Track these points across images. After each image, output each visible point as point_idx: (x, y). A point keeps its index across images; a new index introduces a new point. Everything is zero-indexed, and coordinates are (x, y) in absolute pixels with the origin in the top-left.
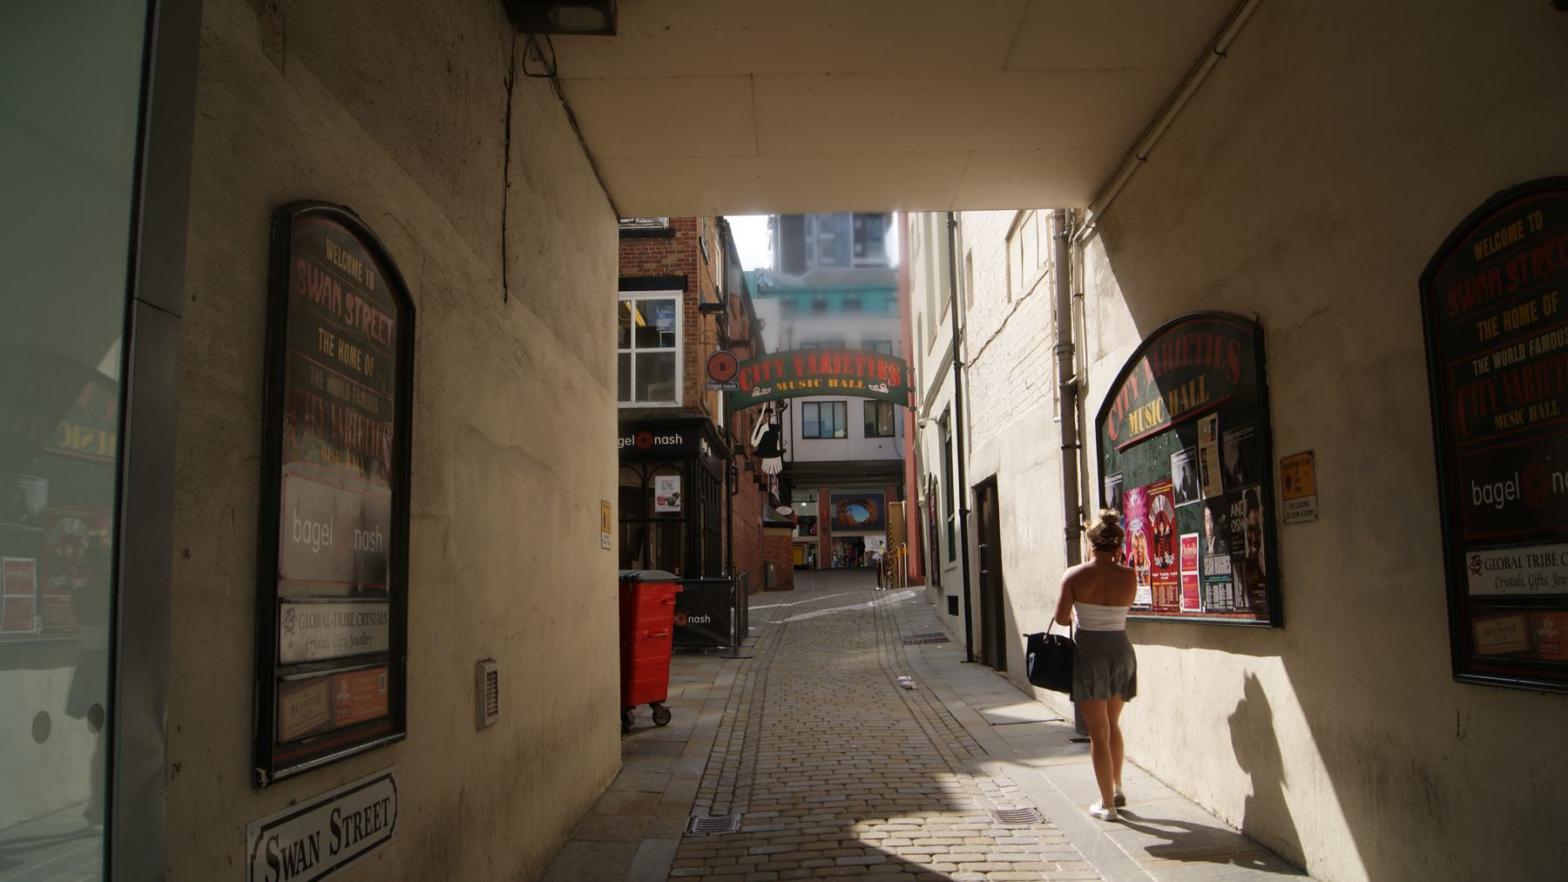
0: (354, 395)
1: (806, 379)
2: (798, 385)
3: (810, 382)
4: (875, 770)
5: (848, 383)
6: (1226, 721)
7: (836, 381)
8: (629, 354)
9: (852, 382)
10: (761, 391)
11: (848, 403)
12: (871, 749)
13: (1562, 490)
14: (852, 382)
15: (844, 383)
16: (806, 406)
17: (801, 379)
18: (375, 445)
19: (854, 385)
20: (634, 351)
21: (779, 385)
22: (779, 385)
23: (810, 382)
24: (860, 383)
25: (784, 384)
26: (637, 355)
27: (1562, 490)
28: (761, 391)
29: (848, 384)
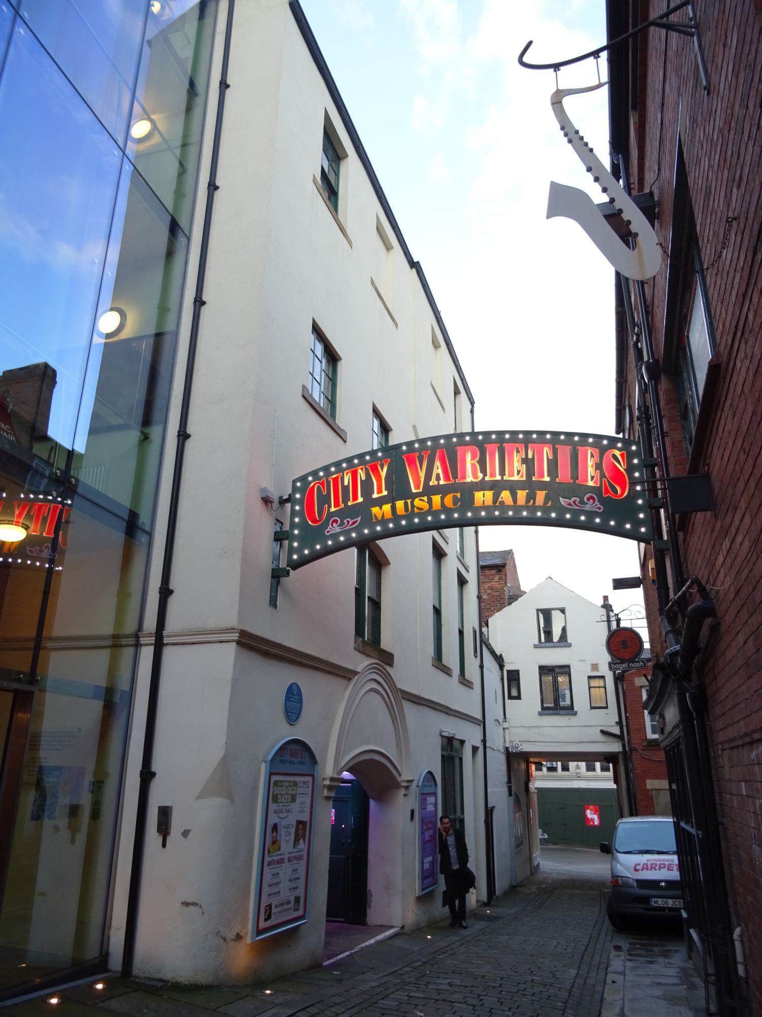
2: (413, 506)
10: (342, 524)
15: (506, 495)
28: (342, 524)
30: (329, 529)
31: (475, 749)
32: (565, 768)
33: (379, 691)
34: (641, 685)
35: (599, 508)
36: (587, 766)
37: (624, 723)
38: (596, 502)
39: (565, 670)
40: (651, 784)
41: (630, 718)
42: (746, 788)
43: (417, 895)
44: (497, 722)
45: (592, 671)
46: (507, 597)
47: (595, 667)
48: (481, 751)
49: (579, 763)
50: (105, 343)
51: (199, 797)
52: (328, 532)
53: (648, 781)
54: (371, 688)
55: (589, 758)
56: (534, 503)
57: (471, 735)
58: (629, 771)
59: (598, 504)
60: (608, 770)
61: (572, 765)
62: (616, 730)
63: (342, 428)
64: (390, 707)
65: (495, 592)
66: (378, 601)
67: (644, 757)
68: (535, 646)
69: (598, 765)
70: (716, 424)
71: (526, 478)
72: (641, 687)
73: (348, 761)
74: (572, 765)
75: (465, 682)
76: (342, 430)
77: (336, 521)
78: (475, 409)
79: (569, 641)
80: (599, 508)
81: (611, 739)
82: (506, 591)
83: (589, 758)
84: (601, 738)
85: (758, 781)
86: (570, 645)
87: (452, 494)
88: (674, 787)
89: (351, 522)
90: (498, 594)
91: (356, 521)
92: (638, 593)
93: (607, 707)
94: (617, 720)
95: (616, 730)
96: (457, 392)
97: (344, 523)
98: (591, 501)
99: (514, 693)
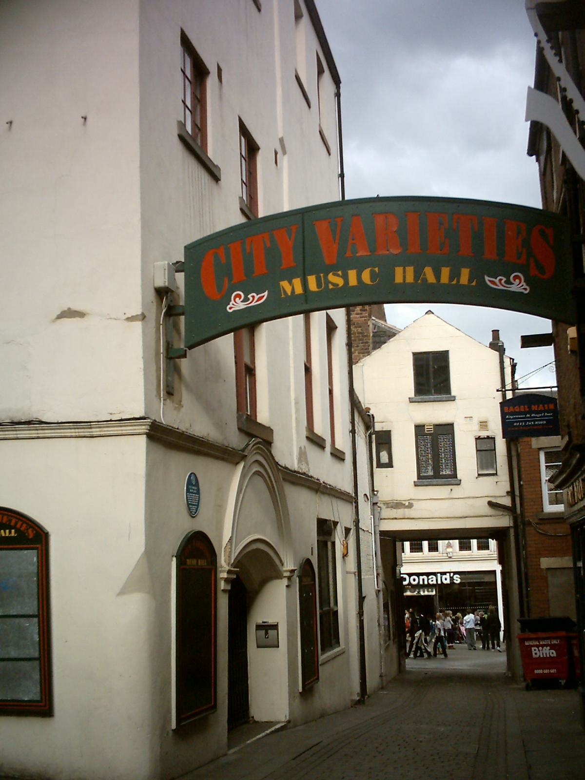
0: (194, 495)
1: (341, 267)
2: (328, 282)
3: (352, 275)
5: (438, 275)
6: (211, 72)
7: (410, 270)
10: (246, 299)
11: (496, 439)
13: (490, 642)
14: (445, 272)
15: (429, 274)
17: (333, 268)
19: (451, 279)
21: (285, 284)
22: (285, 284)
23: (352, 275)
25: (297, 282)
27: (490, 642)
28: (246, 299)
29: (438, 275)
30: (231, 305)
31: (347, 531)
32: (433, 548)
33: (264, 476)
34: (539, 447)
35: (525, 289)
36: (460, 543)
37: (517, 493)
38: (523, 283)
39: (446, 430)
40: (546, 562)
41: (525, 486)
42: (290, 383)
44: (365, 496)
46: (371, 335)
47: (484, 425)
48: (352, 533)
49: (451, 541)
51: (121, 593)
52: (230, 308)
54: (256, 471)
55: (464, 537)
56: (458, 281)
57: (342, 514)
58: (521, 548)
59: (524, 284)
60: (487, 547)
61: (441, 544)
62: (507, 501)
63: (215, 163)
64: (271, 490)
65: (356, 327)
66: (252, 367)
67: (539, 532)
68: (411, 401)
69: (474, 543)
72: (540, 449)
73: (242, 550)
74: (441, 544)
75: (338, 456)
76: (217, 167)
77: (239, 296)
78: (341, 91)
79: (453, 393)
80: (525, 289)
82: (371, 326)
83: (464, 537)
84: (488, 510)
86: (453, 399)
87: (370, 269)
88: (580, 564)
89: (257, 297)
90: (360, 330)
91: (264, 296)
92: (547, 353)
93: (496, 474)
95: (507, 501)
96: (320, 72)
97: (249, 299)
98: (517, 281)
99: (384, 457)
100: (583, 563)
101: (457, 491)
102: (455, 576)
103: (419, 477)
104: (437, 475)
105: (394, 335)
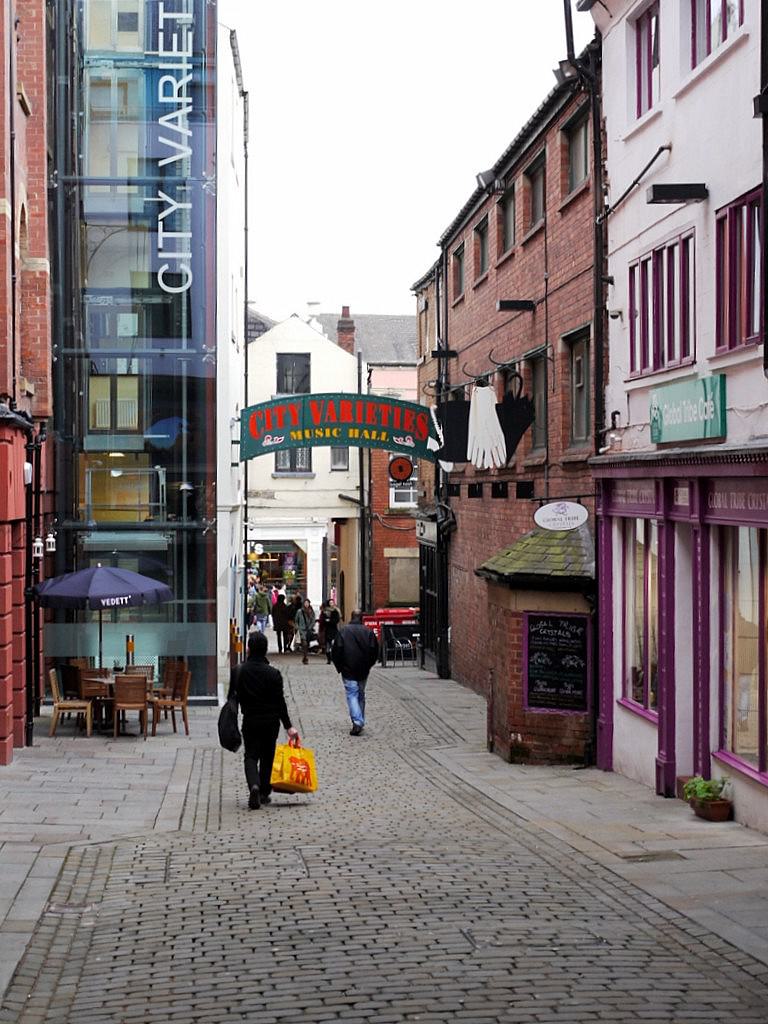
3: (328, 431)
4: (277, 987)
7: (357, 431)
8: (189, 605)
9: (374, 433)
12: (314, 984)
14: (374, 433)
16: (718, 432)
18: (634, 705)
20: (185, 601)
21: (293, 433)
22: (293, 433)
23: (328, 431)
24: (384, 434)
25: (299, 433)
26: (189, 598)
37: (366, 487)
43: (436, 676)
45: (136, 30)
50: (180, 377)
53: (385, 550)
62: (356, 496)
70: (738, 238)
71: (393, 510)
81: (349, 503)
84: (338, 502)
85: (76, 876)
88: (424, 568)
93: (347, 470)
94: (358, 485)
95: (356, 496)
100: (448, 461)
101: (312, 485)
102: (258, 545)
103: (277, 470)
104: (293, 468)
105: (266, 330)
